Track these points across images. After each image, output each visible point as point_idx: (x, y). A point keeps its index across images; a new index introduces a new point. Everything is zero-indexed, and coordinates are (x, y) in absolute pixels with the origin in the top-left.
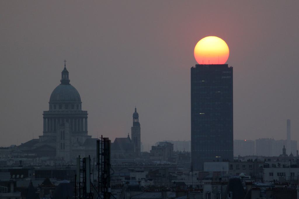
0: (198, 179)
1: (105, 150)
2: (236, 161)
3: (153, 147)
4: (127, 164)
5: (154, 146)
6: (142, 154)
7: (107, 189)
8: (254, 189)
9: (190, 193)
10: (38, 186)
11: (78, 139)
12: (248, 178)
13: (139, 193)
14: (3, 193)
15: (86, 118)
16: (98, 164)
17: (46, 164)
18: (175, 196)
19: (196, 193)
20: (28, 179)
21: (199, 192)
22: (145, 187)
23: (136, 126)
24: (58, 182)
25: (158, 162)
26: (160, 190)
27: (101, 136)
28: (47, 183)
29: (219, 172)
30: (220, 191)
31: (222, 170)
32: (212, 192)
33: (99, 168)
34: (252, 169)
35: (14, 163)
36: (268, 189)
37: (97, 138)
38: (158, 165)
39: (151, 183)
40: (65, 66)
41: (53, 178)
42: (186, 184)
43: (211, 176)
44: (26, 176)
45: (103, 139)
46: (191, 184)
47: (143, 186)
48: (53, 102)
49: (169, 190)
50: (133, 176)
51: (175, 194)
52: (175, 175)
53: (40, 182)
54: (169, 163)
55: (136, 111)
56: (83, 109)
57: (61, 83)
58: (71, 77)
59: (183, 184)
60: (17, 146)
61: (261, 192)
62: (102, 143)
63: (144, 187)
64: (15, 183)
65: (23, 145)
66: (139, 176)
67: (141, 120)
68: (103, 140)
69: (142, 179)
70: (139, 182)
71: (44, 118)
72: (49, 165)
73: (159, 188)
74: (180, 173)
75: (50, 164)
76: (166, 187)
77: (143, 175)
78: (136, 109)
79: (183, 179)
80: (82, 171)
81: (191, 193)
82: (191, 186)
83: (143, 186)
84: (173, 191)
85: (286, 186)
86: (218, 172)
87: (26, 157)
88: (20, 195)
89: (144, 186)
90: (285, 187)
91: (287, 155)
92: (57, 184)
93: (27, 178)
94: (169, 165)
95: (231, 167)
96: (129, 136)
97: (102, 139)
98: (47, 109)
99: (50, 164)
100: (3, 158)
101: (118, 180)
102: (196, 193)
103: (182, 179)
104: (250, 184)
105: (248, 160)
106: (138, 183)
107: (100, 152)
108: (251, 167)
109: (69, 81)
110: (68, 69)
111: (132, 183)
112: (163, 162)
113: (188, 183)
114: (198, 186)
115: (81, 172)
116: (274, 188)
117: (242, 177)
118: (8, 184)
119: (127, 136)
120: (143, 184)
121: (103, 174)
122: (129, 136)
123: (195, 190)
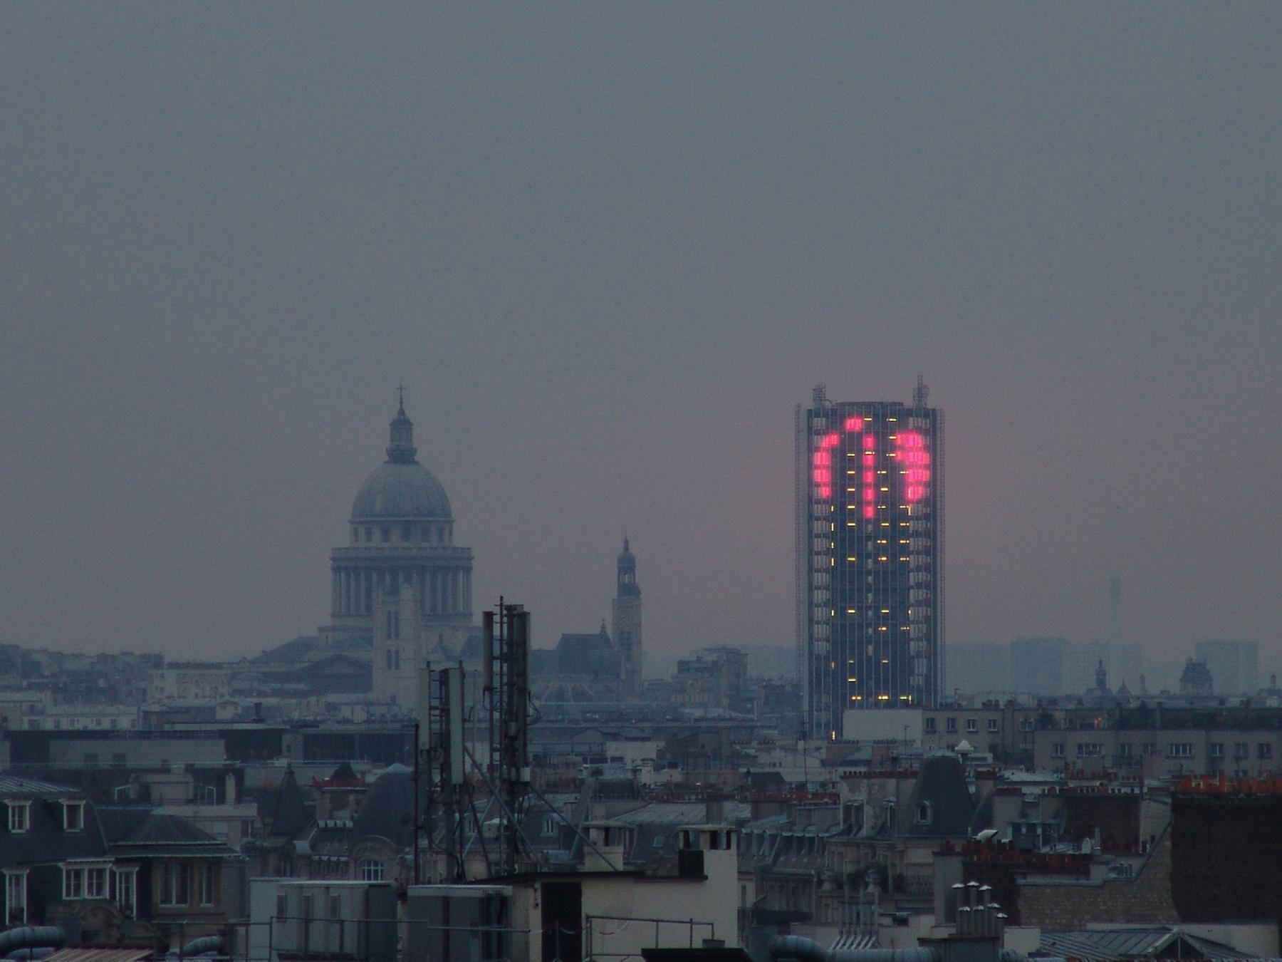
0: (824, 763)
1: (510, 643)
2: (946, 707)
3: (683, 666)
4: (597, 717)
5: (685, 659)
6: (646, 684)
7: (518, 769)
8: (1001, 792)
9: (796, 805)
10: (311, 784)
11: (441, 636)
12: (985, 759)
13: (631, 805)
14: (203, 804)
15: (468, 570)
16: (489, 689)
17: (340, 718)
18: (749, 815)
19: (815, 804)
20: (282, 762)
21: (827, 803)
22: (652, 787)
23: (628, 591)
24: (376, 771)
25: (698, 713)
26: (700, 797)
27: (499, 599)
28: (344, 775)
29: (891, 741)
30: (895, 799)
31: (900, 736)
32: (868, 803)
33: (491, 702)
34: (997, 732)
35: (239, 711)
36: (1046, 792)
37: (687, 946)
38: (696, 720)
39: (676, 775)
40: (401, 403)
41: (362, 758)
42: (787, 779)
43: (864, 755)
44: (276, 752)
45: (505, 609)
46: (802, 778)
47: (648, 783)
48: (365, 519)
49: (730, 797)
50: (617, 754)
51: (750, 809)
52: (752, 752)
53: (325, 773)
54: (734, 714)
55: (626, 548)
56: (460, 538)
57: (386, 458)
58: (420, 438)
59: (777, 778)
60: (249, 659)
61: (1024, 802)
62: (502, 623)
63: (649, 788)
64: (239, 775)
65: (268, 657)
66: (633, 752)
67: (642, 577)
68: (505, 612)
69: (643, 760)
70: (635, 771)
71: (336, 570)
72: (350, 718)
73: (699, 790)
74: (767, 744)
75: (352, 714)
76: (721, 786)
77: (651, 749)
78: (626, 541)
79: (778, 765)
80: (437, 712)
81: (800, 805)
82: (802, 786)
83: (648, 783)
84: (744, 800)
85: (1105, 782)
86: (888, 742)
87: (276, 693)
88: (255, 814)
89: (650, 785)
90: (1101, 784)
91: (1110, 691)
92: (370, 779)
93: (277, 760)
94: (731, 719)
95: (930, 725)
96: (603, 627)
97: (501, 609)
98: (346, 543)
99: (352, 714)
100: (204, 697)
101: (567, 765)
102: (815, 804)
103: (775, 765)
104: (991, 775)
105: (984, 704)
106: (630, 776)
107: (497, 652)
108: (994, 727)
109: (413, 451)
110: (409, 414)
111: (611, 774)
112: (716, 712)
113: (792, 775)
114: (823, 785)
115: (435, 722)
116: (1064, 788)
117: (964, 755)
118: (218, 777)
119: (600, 629)
120: (647, 777)
121: (504, 723)
122: (603, 627)
123: (815, 795)
